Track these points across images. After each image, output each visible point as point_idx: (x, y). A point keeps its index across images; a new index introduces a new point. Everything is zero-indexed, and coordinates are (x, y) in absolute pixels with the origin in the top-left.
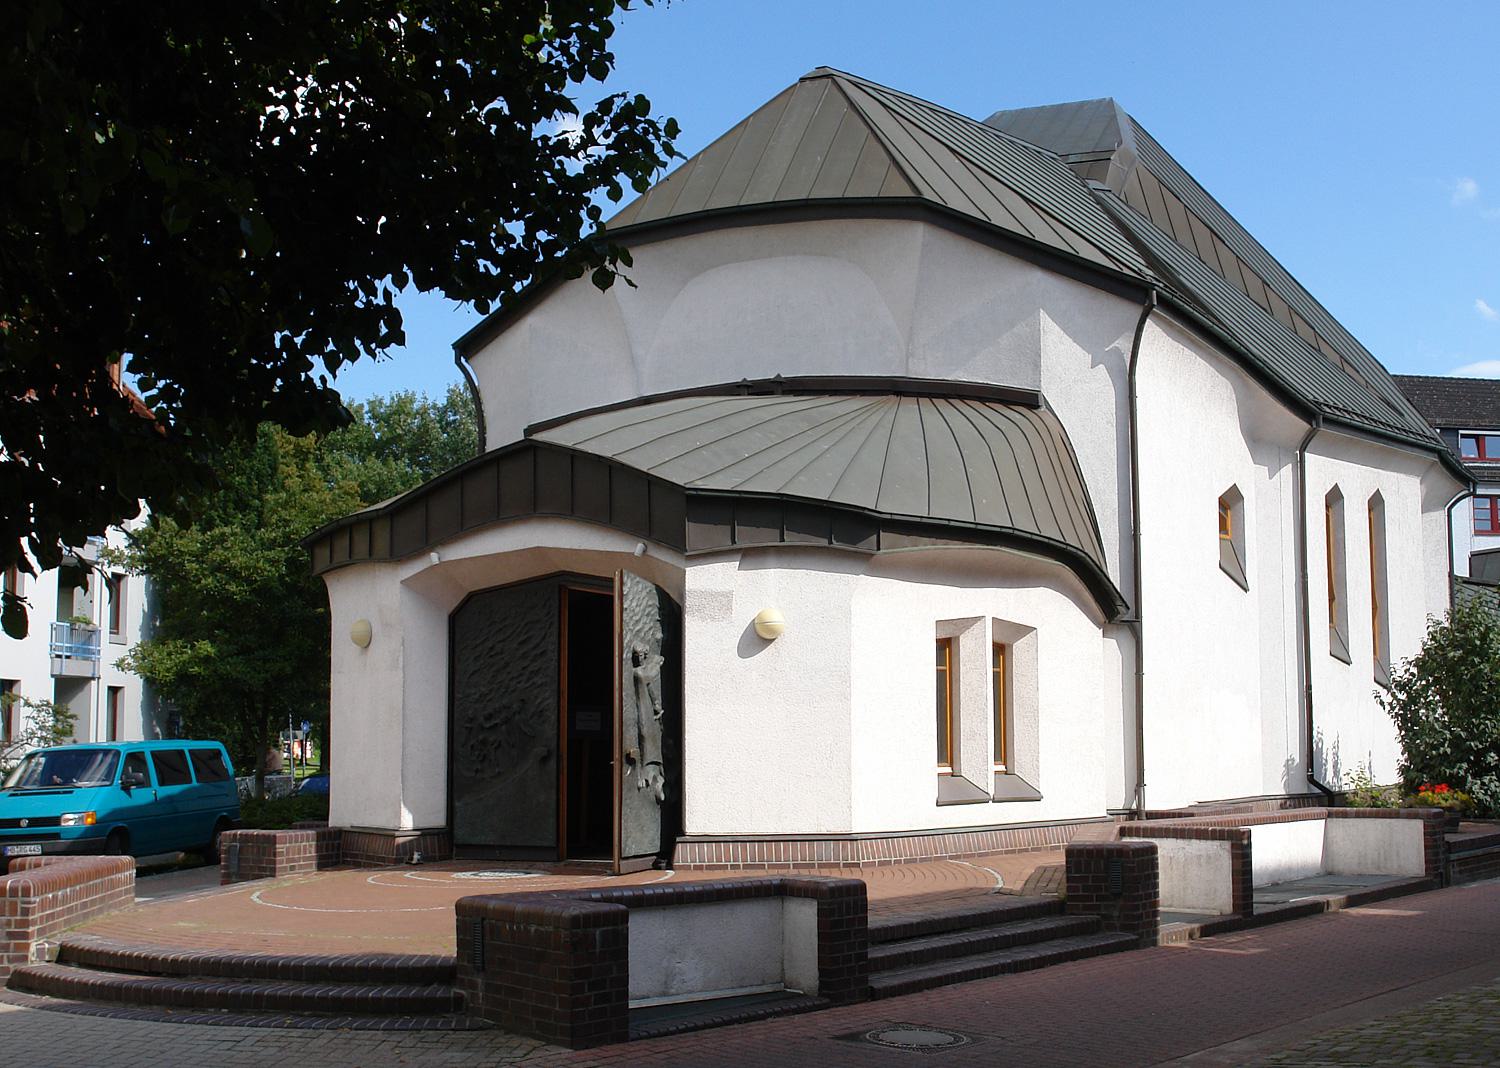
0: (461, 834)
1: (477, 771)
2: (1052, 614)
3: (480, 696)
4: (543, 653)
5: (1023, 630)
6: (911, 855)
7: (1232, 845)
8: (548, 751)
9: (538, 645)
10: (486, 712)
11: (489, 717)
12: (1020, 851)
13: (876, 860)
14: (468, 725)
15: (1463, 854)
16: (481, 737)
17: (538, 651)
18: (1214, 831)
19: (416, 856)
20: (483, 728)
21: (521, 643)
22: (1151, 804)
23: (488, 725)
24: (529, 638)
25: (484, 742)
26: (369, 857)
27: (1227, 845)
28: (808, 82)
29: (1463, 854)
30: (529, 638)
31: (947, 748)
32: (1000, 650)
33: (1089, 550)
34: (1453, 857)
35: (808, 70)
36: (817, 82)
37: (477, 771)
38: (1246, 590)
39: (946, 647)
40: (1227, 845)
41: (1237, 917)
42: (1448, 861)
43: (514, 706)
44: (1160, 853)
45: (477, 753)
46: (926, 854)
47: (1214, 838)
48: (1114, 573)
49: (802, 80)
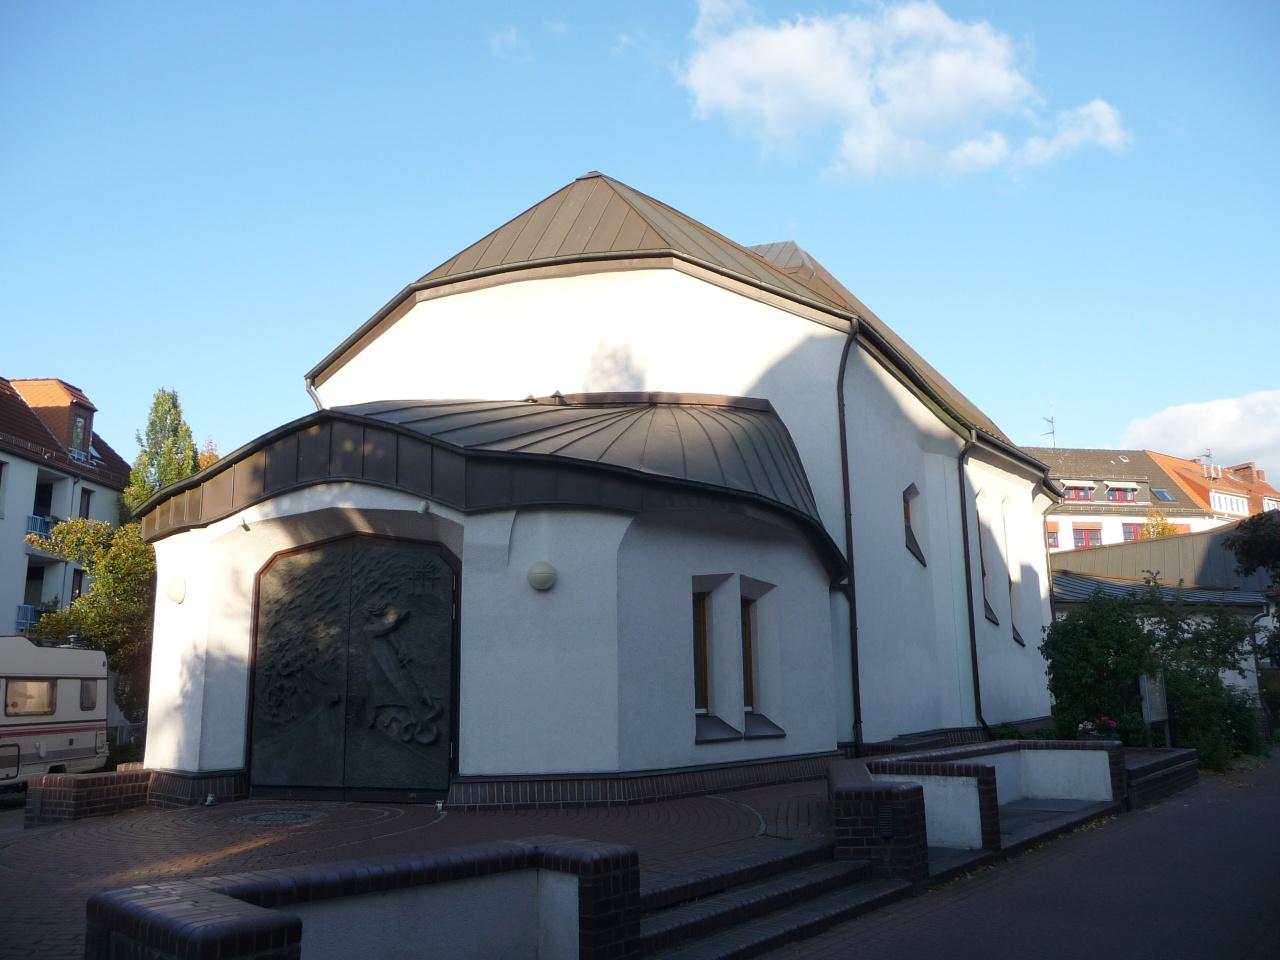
0: (257, 777)
1: (274, 716)
2: (792, 578)
3: (280, 646)
4: (336, 606)
5: (767, 587)
6: (492, 800)
7: (979, 780)
8: (339, 697)
9: (333, 598)
10: (284, 661)
11: (287, 665)
12: (669, 798)
13: (642, 798)
14: (268, 673)
15: (1141, 780)
16: (278, 684)
17: (332, 605)
18: (921, 767)
19: (210, 799)
20: (279, 675)
21: (318, 596)
22: (869, 737)
23: (285, 673)
24: (324, 593)
25: (281, 688)
26: (196, 801)
27: (973, 781)
28: (582, 182)
29: (1141, 780)
30: (324, 593)
31: (702, 696)
32: (747, 604)
33: (802, 508)
34: (1134, 782)
35: (583, 173)
36: (589, 181)
37: (274, 716)
38: (997, 624)
39: (701, 600)
40: (973, 781)
41: (987, 853)
42: (1129, 786)
43: (310, 655)
44: (926, 790)
45: (274, 698)
46: (492, 800)
47: (960, 774)
48: (835, 530)
49: (578, 180)
